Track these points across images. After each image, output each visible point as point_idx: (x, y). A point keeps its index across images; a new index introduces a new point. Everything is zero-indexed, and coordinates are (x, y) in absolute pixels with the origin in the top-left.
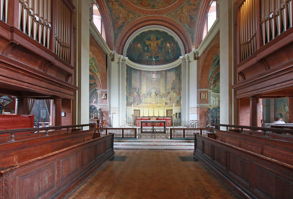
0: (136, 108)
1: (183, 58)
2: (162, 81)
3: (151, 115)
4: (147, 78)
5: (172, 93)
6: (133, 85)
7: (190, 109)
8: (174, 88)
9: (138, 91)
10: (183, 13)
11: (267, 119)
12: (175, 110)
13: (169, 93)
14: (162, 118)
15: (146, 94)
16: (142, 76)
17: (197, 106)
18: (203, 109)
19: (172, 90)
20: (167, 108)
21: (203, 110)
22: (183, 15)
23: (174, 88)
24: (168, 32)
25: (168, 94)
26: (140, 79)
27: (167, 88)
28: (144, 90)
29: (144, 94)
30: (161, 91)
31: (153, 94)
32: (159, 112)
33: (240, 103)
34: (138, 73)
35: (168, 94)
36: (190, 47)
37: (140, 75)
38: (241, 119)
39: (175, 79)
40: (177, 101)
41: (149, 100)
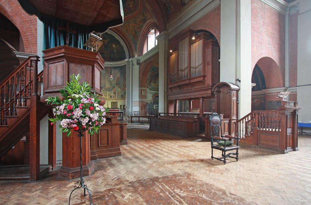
1: (128, 60)
5: (116, 88)
7: (133, 102)
10: (129, 27)
11: (181, 110)
12: (120, 103)
17: (139, 100)
18: (143, 102)
21: (143, 103)
22: (130, 28)
24: (115, 36)
25: (113, 89)
33: (169, 102)
35: (113, 89)
36: (133, 53)
38: (169, 109)
39: (119, 76)
40: (122, 95)
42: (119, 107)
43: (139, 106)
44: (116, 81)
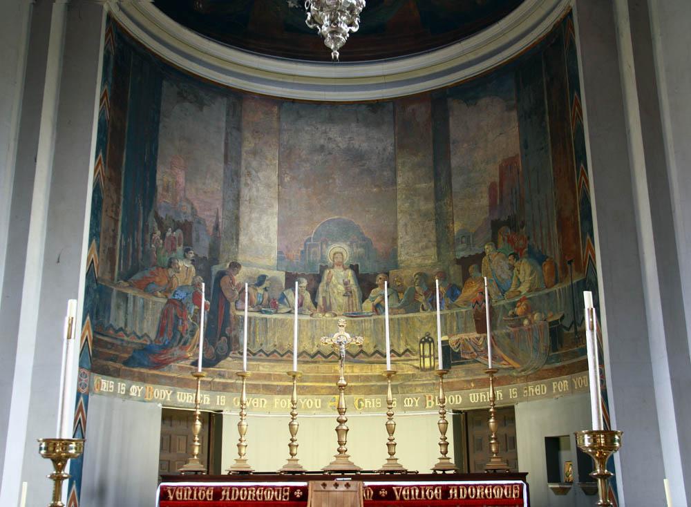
2: (410, 176)
3: (316, 457)
4: (287, 158)
5: (497, 262)
6: (163, 201)
9: (214, 250)
15: (274, 280)
16: (247, 134)
19: (494, 240)
20: (456, 400)
26: (232, 157)
27: (457, 227)
28: (264, 238)
30: (403, 256)
31: (339, 280)
32: (391, 431)
34: (218, 110)
37: (235, 126)
44: (485, 201)
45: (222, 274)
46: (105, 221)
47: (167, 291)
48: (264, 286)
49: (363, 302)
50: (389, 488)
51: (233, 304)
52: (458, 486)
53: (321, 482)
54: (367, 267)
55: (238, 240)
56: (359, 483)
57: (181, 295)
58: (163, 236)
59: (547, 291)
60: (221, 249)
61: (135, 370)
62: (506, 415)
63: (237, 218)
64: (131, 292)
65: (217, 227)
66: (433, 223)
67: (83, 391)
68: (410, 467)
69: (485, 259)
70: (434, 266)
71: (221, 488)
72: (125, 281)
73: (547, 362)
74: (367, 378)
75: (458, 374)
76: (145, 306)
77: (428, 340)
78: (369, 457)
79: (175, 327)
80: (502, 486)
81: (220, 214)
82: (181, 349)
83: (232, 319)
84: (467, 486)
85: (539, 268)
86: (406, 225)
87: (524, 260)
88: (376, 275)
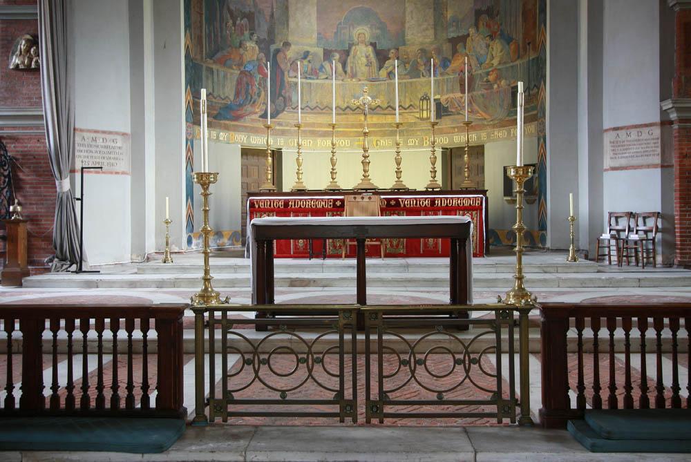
0: (257, 141)
3: (349, 179)
5: (477, 42)
7: (608, 138)
8: (490, 12)
9: (271, 32)
12: (505, 151)
13: (460, 46)
14: (425, 201)
15: (315, 54)
17: (664, 113)
19: (477, 25)
20: (444, 141)
23: (490, 12)
25: (455, 52)
27: (449, 14)
29: (306, 54)
31: (362, 54)
35: (455, 52)
41: (334, 88)
42: (493, 181)
43: (664, 166)
45: (277, 51)
46: (194, 17)
47: (240, 65)
48: (308, 59)
49: (380, 70)
50: (396, 200)
51: (286, 73)
52: (441, 198)
53: (353, 196)
54: (383, 44)
55: (288, 25)
56: (377, 197)
57: (249, 67)
58: (234, 24)
59: (511, 64)
60: (276, 31)
61: (221, 122)
62: (478, 151)
63: (287, 8)
64: (214, 67)
65: (272, 16)
66: (432, 10)
67: (190, 138)
68: (411, 187)
69: (469, 40)
70: (431, 43)
71: (288, 200)
72: (211, 59)
73: (508, 115)
74: (382, 125)
75: (446, 122)
76: (225, 76)
77: (426, 98)
78: (384, 179)
79: (247, 91)
80: (470, 198)
81: (275, 7)
82: (251, 106)
83: (286, 85)
84: (447, 198)
85: (507, 47)
86: (412, 12)
87: (497, 41)
88: (389, 50)
